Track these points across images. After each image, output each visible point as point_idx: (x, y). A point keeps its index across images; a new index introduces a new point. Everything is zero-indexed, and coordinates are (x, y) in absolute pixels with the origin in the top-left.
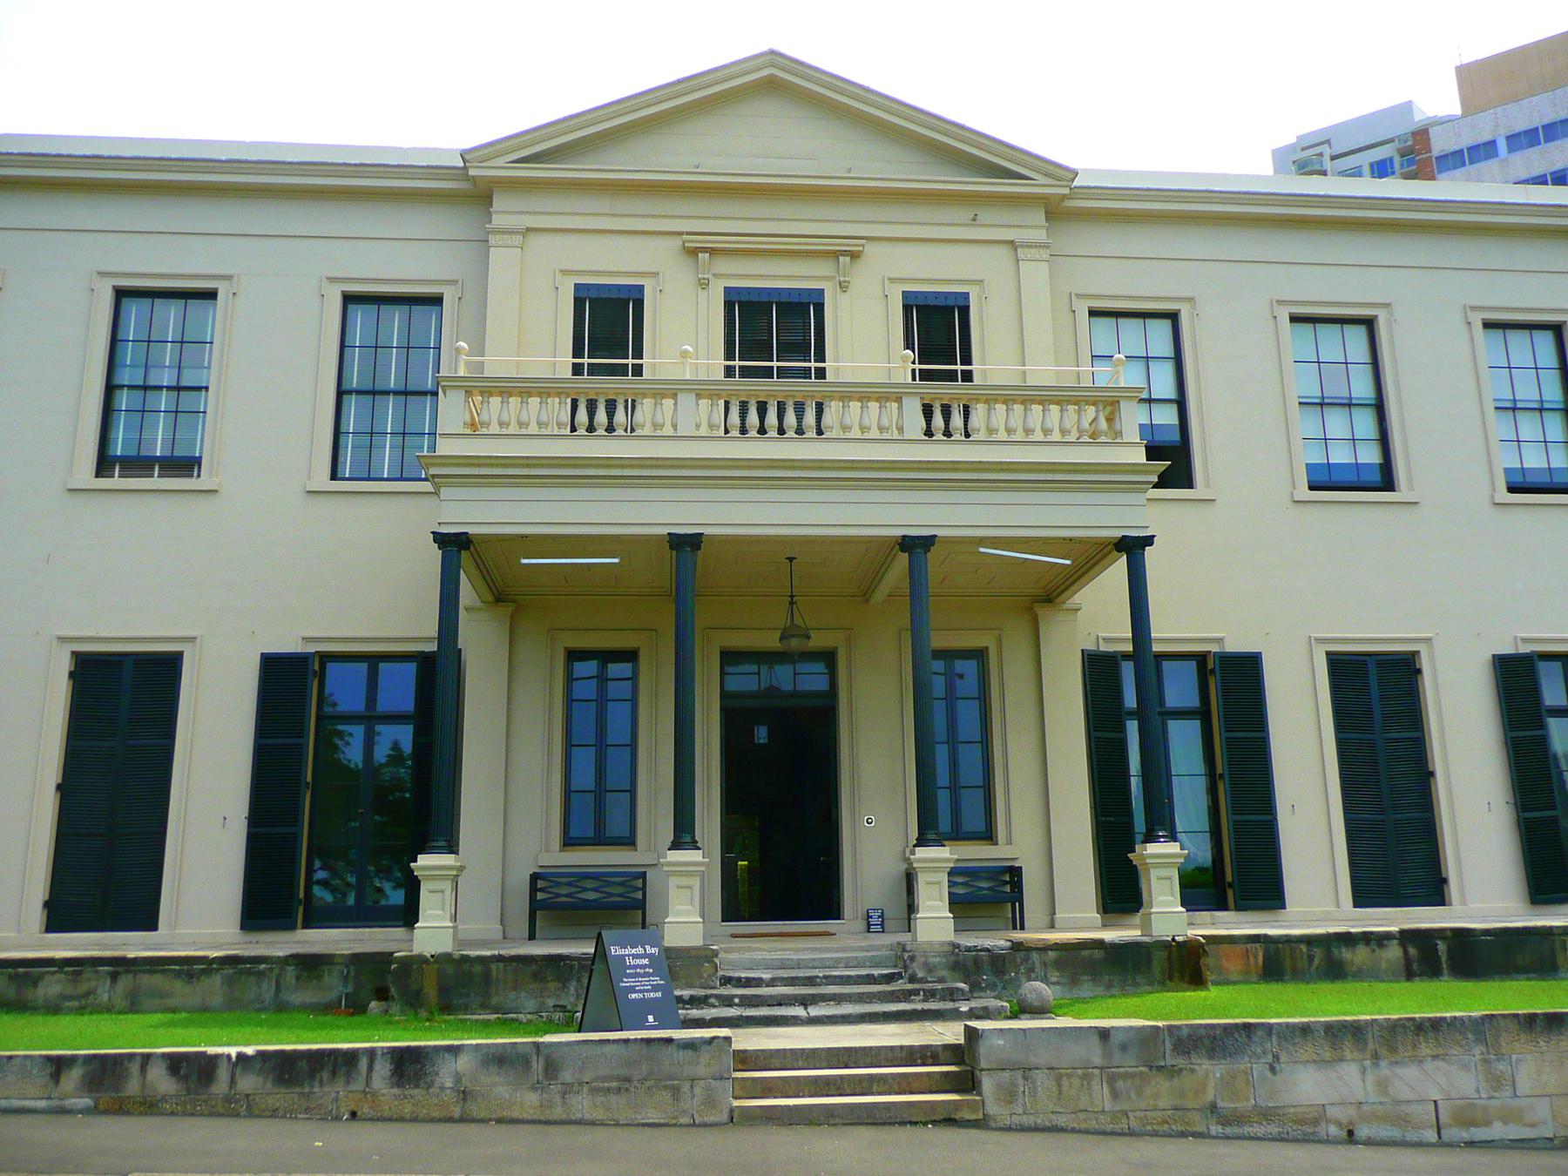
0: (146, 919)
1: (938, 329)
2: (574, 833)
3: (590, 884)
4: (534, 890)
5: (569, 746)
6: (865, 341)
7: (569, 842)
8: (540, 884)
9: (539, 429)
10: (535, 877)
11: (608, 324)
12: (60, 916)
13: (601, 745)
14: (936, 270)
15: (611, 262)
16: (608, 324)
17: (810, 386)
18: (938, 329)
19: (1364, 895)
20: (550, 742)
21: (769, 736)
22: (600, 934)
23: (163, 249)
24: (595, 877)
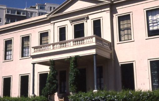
1: (97, 24)
11: (62, 31)
16: (62, 31)
18: (97, 24)
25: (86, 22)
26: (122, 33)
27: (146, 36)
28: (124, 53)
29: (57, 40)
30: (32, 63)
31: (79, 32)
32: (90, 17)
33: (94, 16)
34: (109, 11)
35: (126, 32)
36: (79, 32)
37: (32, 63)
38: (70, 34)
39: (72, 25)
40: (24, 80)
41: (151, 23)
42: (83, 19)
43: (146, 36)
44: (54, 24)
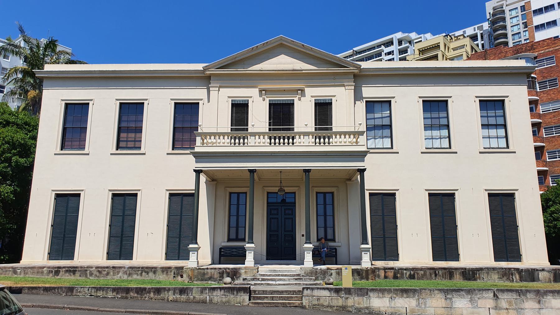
0: (131, 258)
1: (323, 110)
2: (231, 237)
3: (234, 250)
4: (220, 252)
5: (230, 216)
6: (304, 116)
7: (229, 240)
8: (222, 250)
9: (224, 146)
10: (221, 249)
11: (240, 111)
12: (168, 257)
13: (238, 216)
14: (323, 92)
15: (240, 93)
16: (240, 111)
17: (288, 134)
18: (323, 110)
19: (435, 258)
20: (225, 213)
21: (428, 33)
22: (535, 12)
23: (132, 94)
24: (236, 248)
25: (300, 99)
26: (123, 135)
27: (112, 149)
28: (378, 175)
29: (225, 125)
30: (194, 170)
31: (281, 115)
32: (308, 91)
33: (323, 92)
34: (353, 88)
35: (132, 135)
36: (281, 115)
37: (194, 170)
38: (259, 116)
39: (264, 100)
40: (124, 206)
41: (125, 121)
42: (295, 91)
43: (112, 149)
44: (219, 90)
